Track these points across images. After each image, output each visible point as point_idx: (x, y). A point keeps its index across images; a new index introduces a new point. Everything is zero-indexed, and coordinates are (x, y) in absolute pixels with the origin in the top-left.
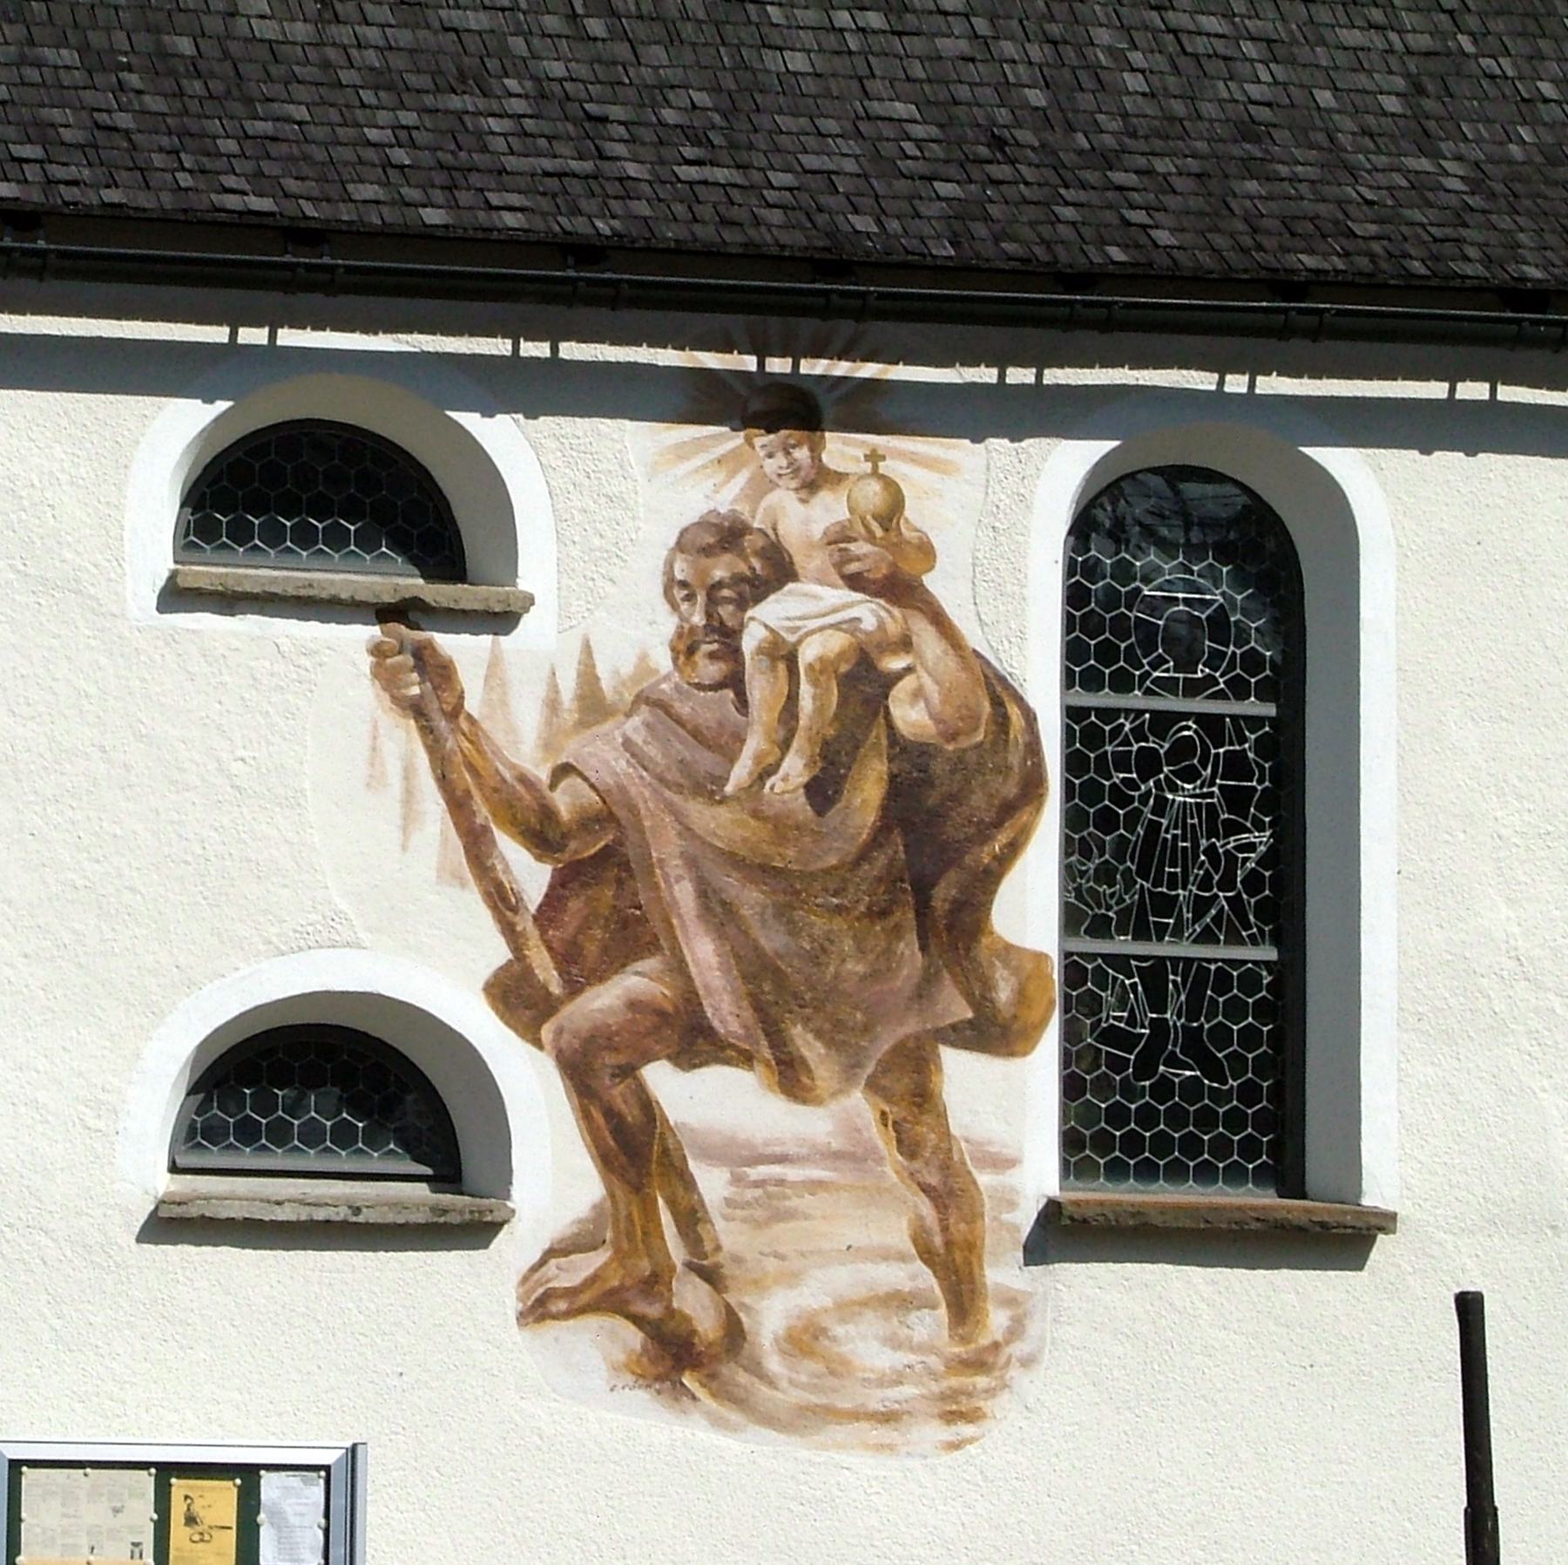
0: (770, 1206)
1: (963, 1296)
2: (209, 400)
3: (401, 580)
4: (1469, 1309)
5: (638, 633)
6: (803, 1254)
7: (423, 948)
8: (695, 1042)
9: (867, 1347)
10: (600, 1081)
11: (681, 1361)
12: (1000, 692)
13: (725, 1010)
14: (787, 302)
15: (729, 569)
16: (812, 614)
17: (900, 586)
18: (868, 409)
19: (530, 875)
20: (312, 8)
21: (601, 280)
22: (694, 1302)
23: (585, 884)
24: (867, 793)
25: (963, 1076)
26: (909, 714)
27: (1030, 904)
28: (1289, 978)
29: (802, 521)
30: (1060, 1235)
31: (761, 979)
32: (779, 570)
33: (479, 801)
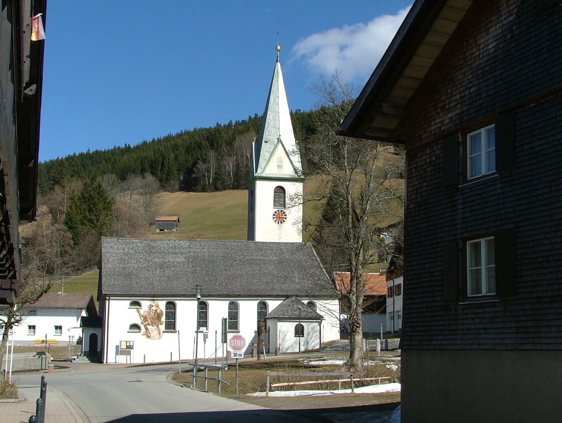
0: (152, 331)
2: (394, 12)
3: (139, 307)
7: (138, 321)
8: (149, 325)
9: (156, 336)
11: (148, 337)
14: (153, 296)
15: (151, 306)
16: (154, 308)
18: (156, 300)
19: (142, 318)
21: (145, 296)
23: (145, 319)
25: (160, 326)
27: (163, 319)
29: (154, 304)
30: (164, 332)
31: (151, 322)
33: (140, 316)
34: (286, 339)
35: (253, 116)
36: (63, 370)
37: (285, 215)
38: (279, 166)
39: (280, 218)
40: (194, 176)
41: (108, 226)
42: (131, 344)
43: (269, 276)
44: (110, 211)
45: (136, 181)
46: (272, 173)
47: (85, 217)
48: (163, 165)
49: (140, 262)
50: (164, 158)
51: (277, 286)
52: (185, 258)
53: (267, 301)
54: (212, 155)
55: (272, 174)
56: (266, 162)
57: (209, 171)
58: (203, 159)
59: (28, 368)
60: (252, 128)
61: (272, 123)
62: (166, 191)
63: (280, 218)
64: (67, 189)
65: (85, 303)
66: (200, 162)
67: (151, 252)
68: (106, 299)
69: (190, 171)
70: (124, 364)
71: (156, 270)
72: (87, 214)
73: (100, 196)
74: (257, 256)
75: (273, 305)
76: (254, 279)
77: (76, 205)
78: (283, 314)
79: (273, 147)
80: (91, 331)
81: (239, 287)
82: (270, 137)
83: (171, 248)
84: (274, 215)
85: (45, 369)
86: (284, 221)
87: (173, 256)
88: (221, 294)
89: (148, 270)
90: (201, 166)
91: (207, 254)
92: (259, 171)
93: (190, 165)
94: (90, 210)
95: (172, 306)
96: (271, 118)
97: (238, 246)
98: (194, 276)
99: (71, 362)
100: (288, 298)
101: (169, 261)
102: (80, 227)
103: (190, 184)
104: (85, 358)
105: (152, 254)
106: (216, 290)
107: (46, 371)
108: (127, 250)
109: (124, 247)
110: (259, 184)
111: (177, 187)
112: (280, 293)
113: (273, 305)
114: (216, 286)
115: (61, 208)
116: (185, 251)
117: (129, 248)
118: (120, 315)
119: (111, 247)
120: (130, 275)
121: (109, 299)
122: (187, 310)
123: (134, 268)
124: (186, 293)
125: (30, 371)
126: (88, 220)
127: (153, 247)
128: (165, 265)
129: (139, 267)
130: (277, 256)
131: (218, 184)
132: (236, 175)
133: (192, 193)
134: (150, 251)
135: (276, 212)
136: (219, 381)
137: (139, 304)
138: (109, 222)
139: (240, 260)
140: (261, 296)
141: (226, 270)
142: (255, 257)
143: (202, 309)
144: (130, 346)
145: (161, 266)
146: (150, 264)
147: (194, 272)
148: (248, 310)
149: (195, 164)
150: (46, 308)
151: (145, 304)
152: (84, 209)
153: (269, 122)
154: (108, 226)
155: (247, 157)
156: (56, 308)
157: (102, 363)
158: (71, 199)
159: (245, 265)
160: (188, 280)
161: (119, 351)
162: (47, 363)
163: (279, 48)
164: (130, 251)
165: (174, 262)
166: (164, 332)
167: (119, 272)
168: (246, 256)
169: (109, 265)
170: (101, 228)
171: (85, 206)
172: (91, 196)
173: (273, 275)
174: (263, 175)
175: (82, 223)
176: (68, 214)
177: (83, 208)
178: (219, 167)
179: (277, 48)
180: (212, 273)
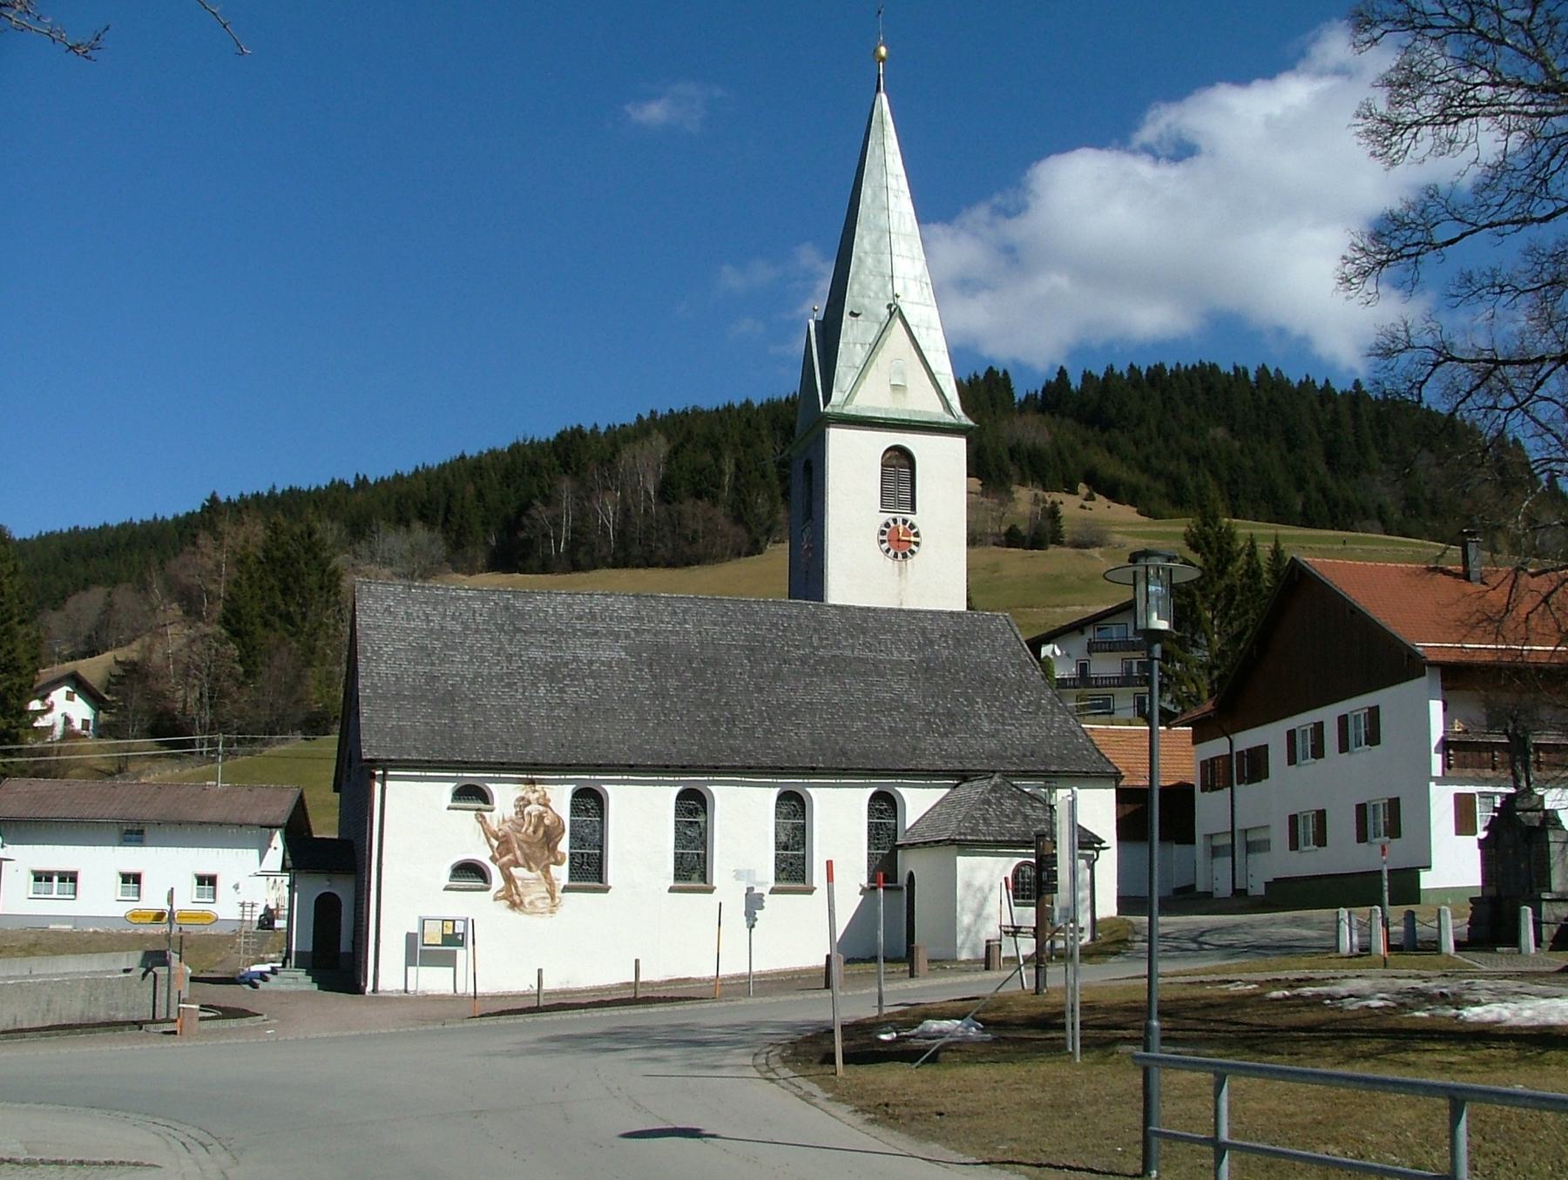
0: (527, 886)
1: (553, 898)
3: (482, 805)
4: (637, 961)
5: (511, 812)
6: (941, 1114)
7: (481, 853)
8: (517, 865)
9: (539, 904)
10: (504, 870)
11: (514, 905)
12: (559, 818)
13: (521, 861)
14: (531, 769)
15: (523, 803)
16: (534, 809)
17: (546, 805)
18: (541, 782)
19: (495, 843)
20: (1565, 78)
22: (516, 898)
23: (503, 844)
24: (541, 832)
26: (547, 822)
27: (564, 846)
28: (601, 855)
29: (533, 797)
30: (566, 889)
32: (529, 803)
33: (489, 834)
34: (986, 912)
35: (646, 417)
36: (233, 1023)
37: (917, 535)
38: (895, 387)
39: (900, 543)
40: (522, 535)
41: (331, 631)
42: (460, 928)
43: (897, 708)
44: (336, 594)
45: (392, 541)
46: (874, 404)
47: (273, 608)
48: (448, 510)
49: (483, 660)
50: (451, 495)
51: (928, 743)
52: (625, 648)
53: (901, 790)
54: (566, 485)
55: (876, 409)
56: (854, 374)
57: (557, 525)
58: (545, 496)
59: (102, 1016)
60: (655, 432)
61: (869, 261)
62: (456, 570)
63: (900, 543)
64: (228, 541)
65: (281, 811)
66: (537, 503)
67: (519, 630)
68: (373, 776)
69: (512, 526)
70: (441, 999)
71: (534, 684)
72: (279, 600)
73: (310, 556)
74: (853, 647)
75: (917, 802)
76: (852, 720)
77: (251, 577)
78: (974, 831)
79: (875, 330)
80: (319, 885)
81: (808, 744)
82: (866, 301)
83: (580, 618)
84: (883, 533)
85: (168, 1020)
86: (912, 552)
87: (587, 641)
88: (752, 763)
89: (509, 685)
90: (540, 511)
91: (694, 640)
92: (836, 397)
93: (511, 511)
94: (286, 591)
95: (591, 803)
96: (867, 247)
97: (790, 617)
98: (662, 705)
99: (255, 986)
100: (965, 779)
101: (576, 659)
102: (260, 631)
103: (512, 556)
104: (301, 973)
105: (518, 636)
106: (735, 751)
107: (169, 1027)
108: (437, 619)
109: (428, 610)
110: (837, 438)
111: (481, 561)
112: (940, 764)
113: (917, 802)
114: (735, 738)
115: (212, 587)
116: (625, 628)
117: (444, 616)
118: (420, 829)
119: (388, 609)
120: (449, 699)
121: (384, 779)
122: (641, 815)
123: (463, 677)
124: (639, 761)
125: (112, 1025)
126: (280, 616)
127: (521, 615)
128: (565, 671)
129: (477, 675)
130: (913, 651)
131: (580, 556)
132: (621, 534)
133: (518, 575)
134: (515, 624)
135: (887, 525)
136: (1220, 1149)
137: (483, 796)
138: (332, 621)
139: (804, 662)
140: (882, 773)
141: (760, 690)
142: (848, 653)
143: (690, 812)
144: (455, 935)
145: (552, 674)
146: (515, 666)
147: (661, 694)
148: (841, 814)
149: (524, 508)
150: (173, 823)
151: (505, 795)
152: (272, 588)
153: (859, 259)
154: (331, 631)
155: (647, 492)
156: (201, 823)
157: (360, 991)
158: (241, 562)
159: (818, 675)
160: (642, 720)
161: (417, 952)
162: (174, 995)
163: (883, 51)
164: (450, 624)
165: (591, 662)
166: (566, 889)
167: (414, 688)
168: (817, 649)
169: (383, 667)
170: (313, 635)
171: (272, 581)
172: (288, 555)
173: (908, 707)
174: (850, 410)
175: (266, 624)
176: (232, 598)
177: (266, 585)
178: (582, 515)
179: (876, 51)
180: (718, 699)
